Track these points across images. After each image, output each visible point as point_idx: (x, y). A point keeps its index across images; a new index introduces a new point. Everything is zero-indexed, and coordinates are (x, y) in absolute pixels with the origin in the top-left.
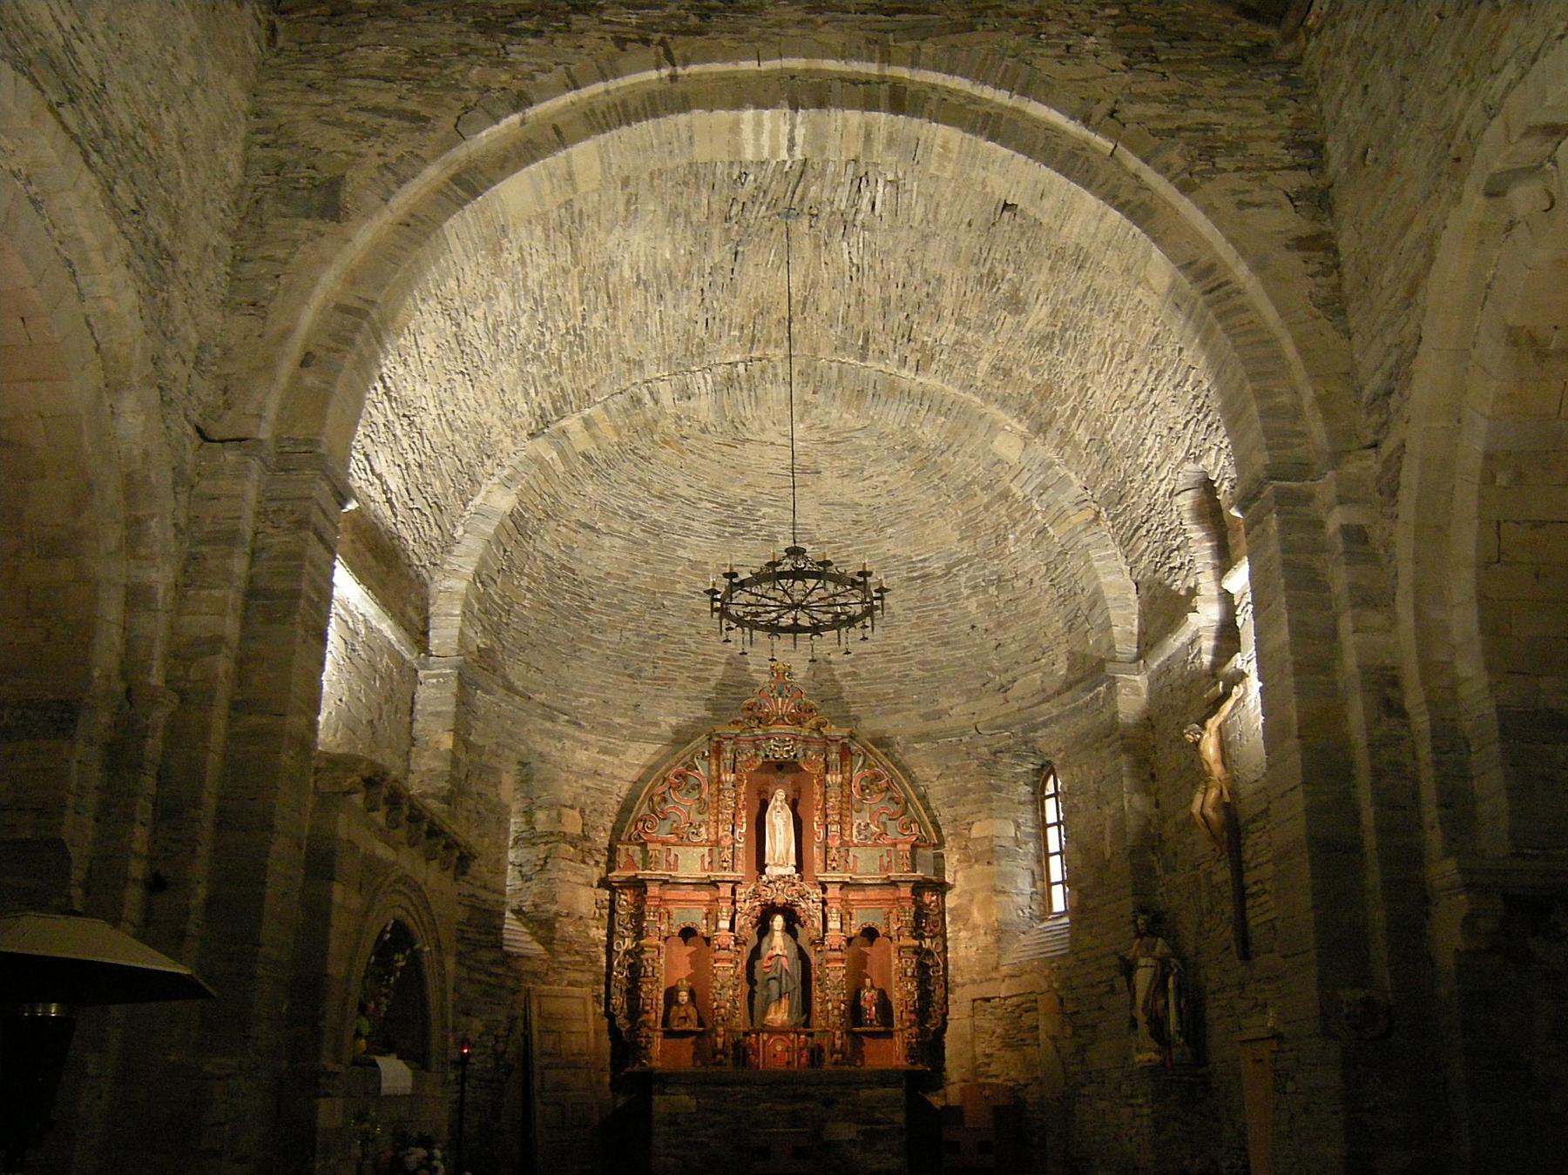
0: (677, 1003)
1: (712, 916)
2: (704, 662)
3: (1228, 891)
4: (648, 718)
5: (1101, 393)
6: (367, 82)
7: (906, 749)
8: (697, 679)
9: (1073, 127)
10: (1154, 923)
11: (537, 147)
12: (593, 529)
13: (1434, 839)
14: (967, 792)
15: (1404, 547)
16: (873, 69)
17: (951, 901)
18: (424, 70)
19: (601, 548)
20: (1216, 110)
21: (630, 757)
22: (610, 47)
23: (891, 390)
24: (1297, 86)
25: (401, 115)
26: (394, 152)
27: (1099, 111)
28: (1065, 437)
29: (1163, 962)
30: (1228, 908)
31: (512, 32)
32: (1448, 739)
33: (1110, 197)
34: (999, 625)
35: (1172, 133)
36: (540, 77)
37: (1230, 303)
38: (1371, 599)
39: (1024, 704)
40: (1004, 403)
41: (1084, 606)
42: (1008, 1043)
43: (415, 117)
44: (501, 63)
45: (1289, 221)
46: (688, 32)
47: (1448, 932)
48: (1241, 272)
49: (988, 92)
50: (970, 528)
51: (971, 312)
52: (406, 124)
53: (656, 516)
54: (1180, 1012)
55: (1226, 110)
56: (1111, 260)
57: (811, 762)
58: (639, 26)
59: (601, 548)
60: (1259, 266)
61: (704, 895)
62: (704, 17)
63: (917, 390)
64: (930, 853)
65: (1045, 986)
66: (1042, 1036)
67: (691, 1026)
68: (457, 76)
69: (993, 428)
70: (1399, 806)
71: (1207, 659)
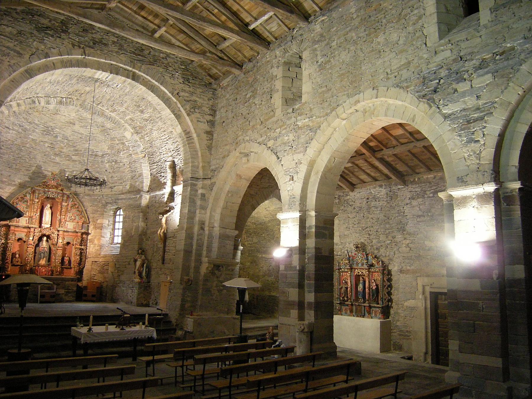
0: (15, 257)
1: (28, 235)
2: (30, 166)
3: (162, 249)
4: (12, 179)
5: (155, 134)
6: (5, 38)
7: (83, 197)
8: (27, 170)
9: (169, 94)
10: (142, 251)
11: (48, 68)
12: (8, 128)
13: (204, 253)
14: (98, 211)
15: (211, 200)
16: (131, 69)
17: (90, 237)
18: (22, 38)
19: (9, 133)
20: (198, 97)
21: (6, 190)
22: (71, 46)
23: (102, 114)
24: (215, 97)
25: (15, 51)
26: (13, 62)
27: (176, 92)
28: (142, 137)
29: (143, 260)
30: (161, 253)
31: (46, 33)
32: (210, 236)
33: (173, 112)
34: (113, 172)
35: (188, 101)
36: (52, 50)
37: (191, 141)
38: (203, 208)
39: (116, 193)
40: (130, 125)
41: (137, 175)
42: (100, 272)
43: (18, 53)
44: (42, 41)
45: (206, 127)
46: (90, 47)
47: (204, 269)
48: (195, 135)
49: (154, 81)
50: (111, 147)
51: (130, 109)
52: (16, 54)
53: (27, 127)
54: (146, 272)
55: (200, 98)
56: (169, 122)
57: (59, 198)
58: (78, 42)
59: (9, 133)
60: (198, 136)
61: (26, 230)
62: (94, 44)
63: (109, 116)
64: (86, 225)
65: (111, 260)
66: (109, 272)
67: (19, 263)
68: (30, 43)
69: (125, 129)
70: (200, 246)
71: (166, 200)
